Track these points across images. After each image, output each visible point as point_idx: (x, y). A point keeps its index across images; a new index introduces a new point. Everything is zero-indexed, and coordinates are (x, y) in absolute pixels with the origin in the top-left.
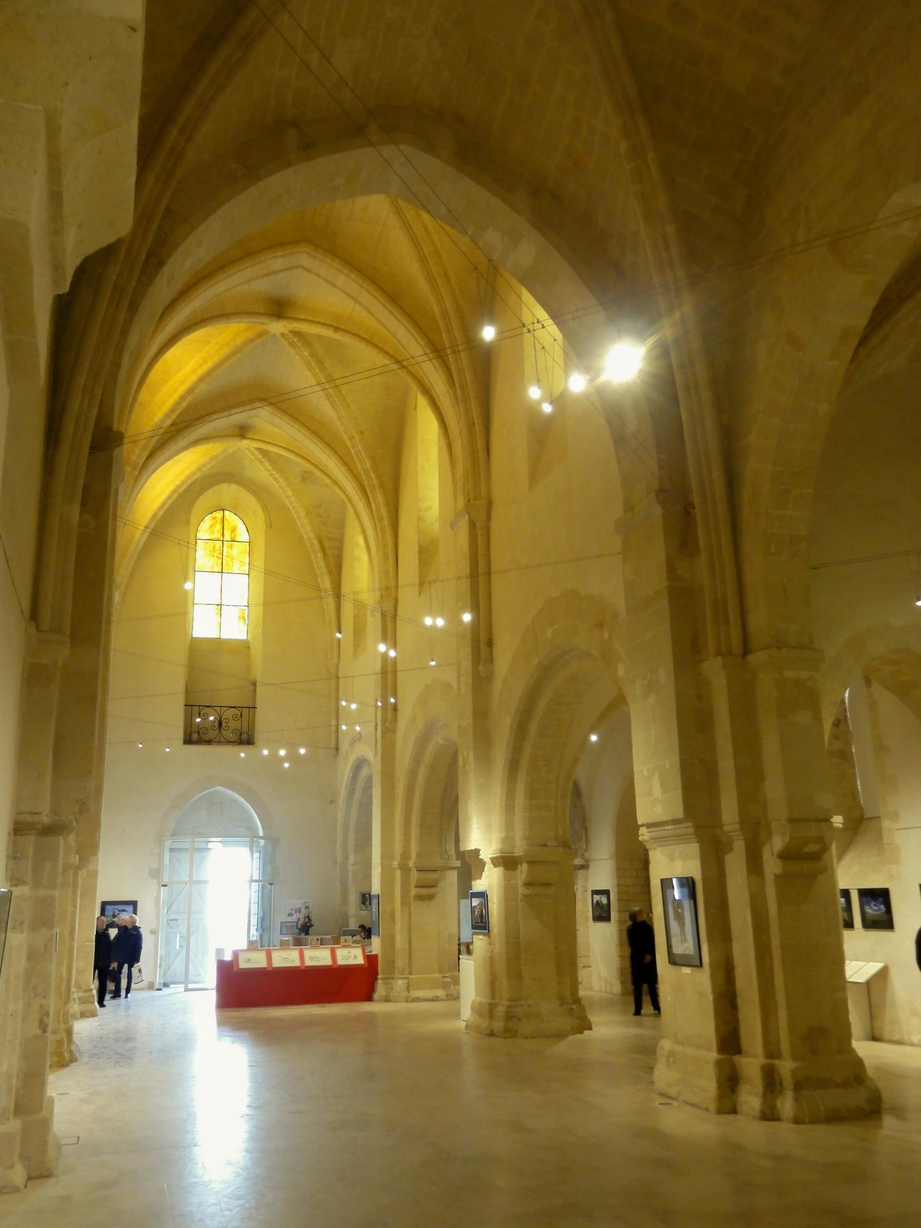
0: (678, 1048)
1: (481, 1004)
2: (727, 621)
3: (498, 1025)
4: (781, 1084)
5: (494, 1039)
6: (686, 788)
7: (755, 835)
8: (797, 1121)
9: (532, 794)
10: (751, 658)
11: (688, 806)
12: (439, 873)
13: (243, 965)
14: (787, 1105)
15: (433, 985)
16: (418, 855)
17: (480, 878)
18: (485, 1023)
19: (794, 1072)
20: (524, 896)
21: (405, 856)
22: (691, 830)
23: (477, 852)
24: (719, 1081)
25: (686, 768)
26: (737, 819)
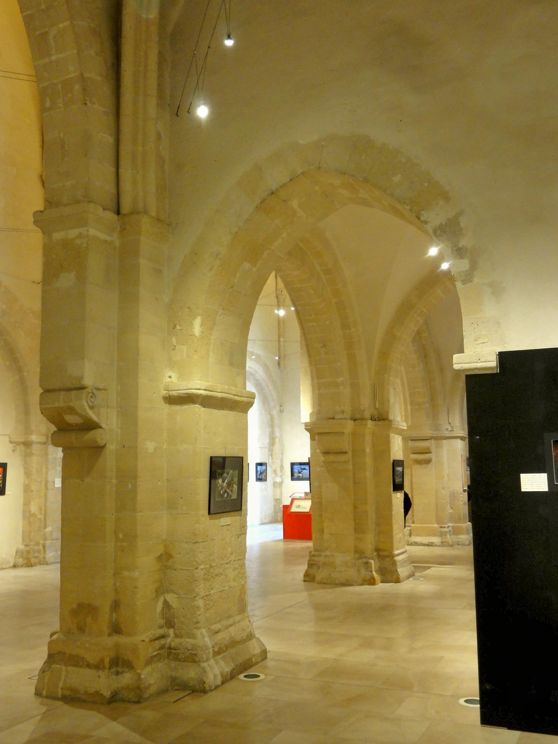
13: (294, 509)
15: (432, 533)
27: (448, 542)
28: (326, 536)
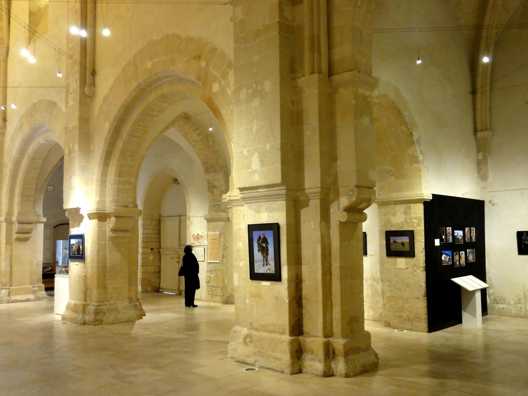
0: (254, 333)
1: (75, 305)
2: (319, 52)
3: (89, 317)
4: (334, 353)
5: (87, 327)
6: (284, 162)
7: (328, 195)
8: (347, 376)
9: (120, 174)
10: (336, 78)
11: (284, 176)
12: (33, 225)
14: (340, 366)
16: (19, 213)
17: (79, 225)
18: (80, 316)
19: (345, 345)
20: (110, 237)
21: (9, 214)
22: (284, 192)
23: (77, 210)
24: (291, 353)
25: (284, 149)
26: (319, 185)
27: (39, 297)
28: (109, 290)
